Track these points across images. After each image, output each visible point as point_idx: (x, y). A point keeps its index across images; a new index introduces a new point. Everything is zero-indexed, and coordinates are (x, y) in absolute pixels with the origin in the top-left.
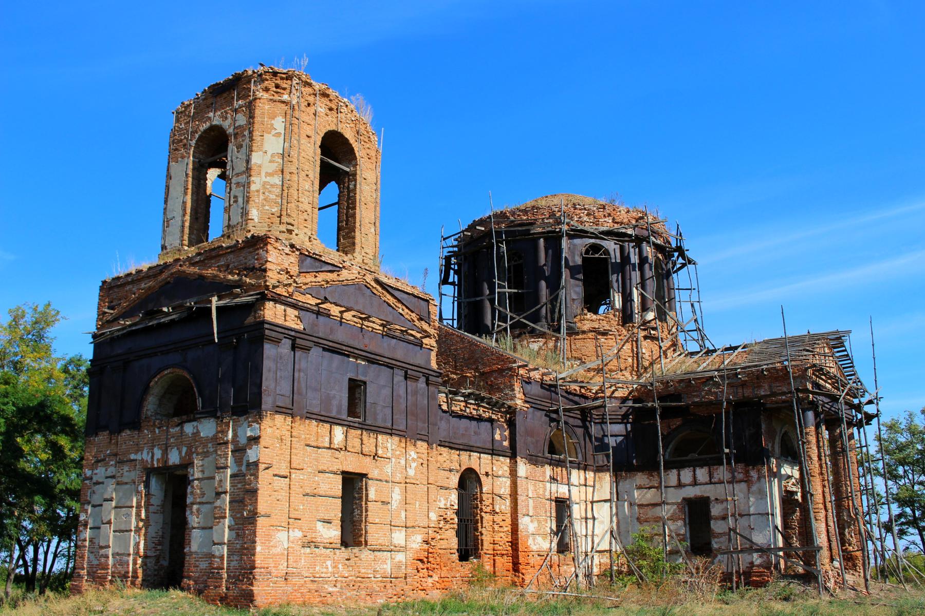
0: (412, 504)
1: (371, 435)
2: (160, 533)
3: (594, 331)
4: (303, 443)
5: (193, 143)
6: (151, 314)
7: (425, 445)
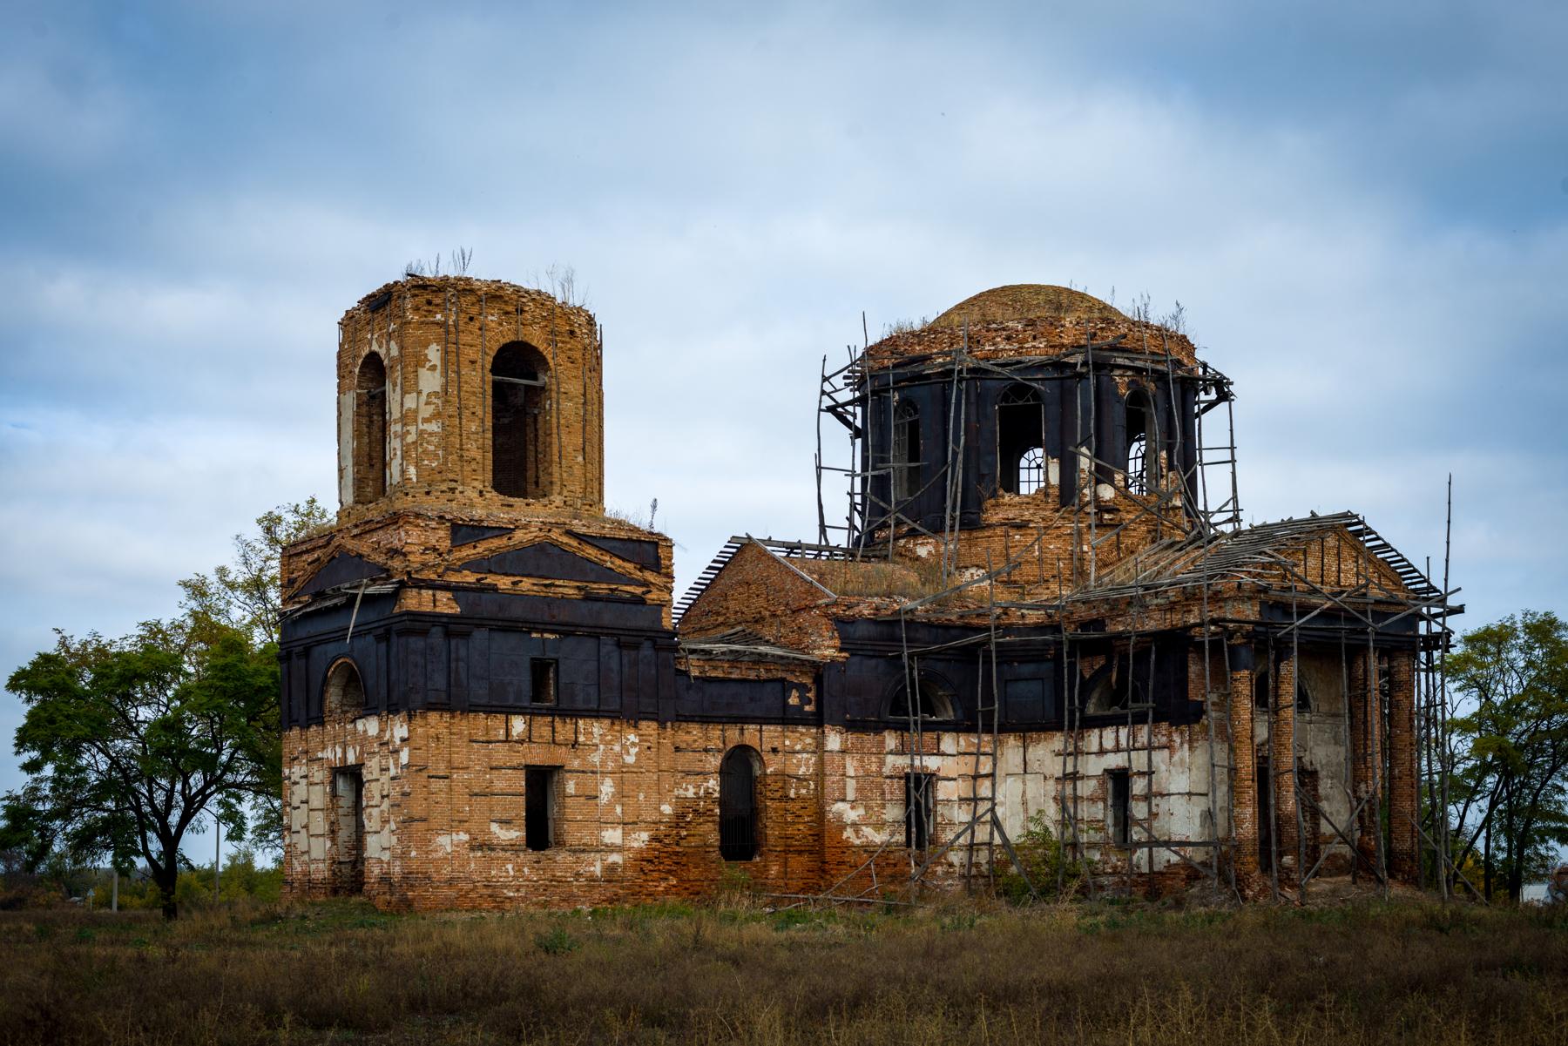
0: (633, 797)
1: (568, 721)
2: (354, 837)
3: (1006, 524)
4: (466, 739)
5: (357, 370)
6: (319, 595)
7: (654, 725)
